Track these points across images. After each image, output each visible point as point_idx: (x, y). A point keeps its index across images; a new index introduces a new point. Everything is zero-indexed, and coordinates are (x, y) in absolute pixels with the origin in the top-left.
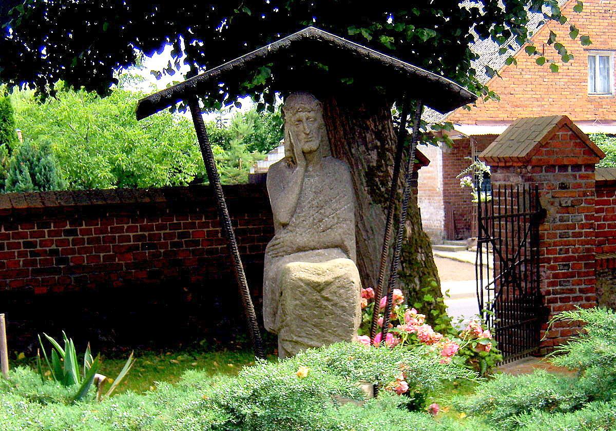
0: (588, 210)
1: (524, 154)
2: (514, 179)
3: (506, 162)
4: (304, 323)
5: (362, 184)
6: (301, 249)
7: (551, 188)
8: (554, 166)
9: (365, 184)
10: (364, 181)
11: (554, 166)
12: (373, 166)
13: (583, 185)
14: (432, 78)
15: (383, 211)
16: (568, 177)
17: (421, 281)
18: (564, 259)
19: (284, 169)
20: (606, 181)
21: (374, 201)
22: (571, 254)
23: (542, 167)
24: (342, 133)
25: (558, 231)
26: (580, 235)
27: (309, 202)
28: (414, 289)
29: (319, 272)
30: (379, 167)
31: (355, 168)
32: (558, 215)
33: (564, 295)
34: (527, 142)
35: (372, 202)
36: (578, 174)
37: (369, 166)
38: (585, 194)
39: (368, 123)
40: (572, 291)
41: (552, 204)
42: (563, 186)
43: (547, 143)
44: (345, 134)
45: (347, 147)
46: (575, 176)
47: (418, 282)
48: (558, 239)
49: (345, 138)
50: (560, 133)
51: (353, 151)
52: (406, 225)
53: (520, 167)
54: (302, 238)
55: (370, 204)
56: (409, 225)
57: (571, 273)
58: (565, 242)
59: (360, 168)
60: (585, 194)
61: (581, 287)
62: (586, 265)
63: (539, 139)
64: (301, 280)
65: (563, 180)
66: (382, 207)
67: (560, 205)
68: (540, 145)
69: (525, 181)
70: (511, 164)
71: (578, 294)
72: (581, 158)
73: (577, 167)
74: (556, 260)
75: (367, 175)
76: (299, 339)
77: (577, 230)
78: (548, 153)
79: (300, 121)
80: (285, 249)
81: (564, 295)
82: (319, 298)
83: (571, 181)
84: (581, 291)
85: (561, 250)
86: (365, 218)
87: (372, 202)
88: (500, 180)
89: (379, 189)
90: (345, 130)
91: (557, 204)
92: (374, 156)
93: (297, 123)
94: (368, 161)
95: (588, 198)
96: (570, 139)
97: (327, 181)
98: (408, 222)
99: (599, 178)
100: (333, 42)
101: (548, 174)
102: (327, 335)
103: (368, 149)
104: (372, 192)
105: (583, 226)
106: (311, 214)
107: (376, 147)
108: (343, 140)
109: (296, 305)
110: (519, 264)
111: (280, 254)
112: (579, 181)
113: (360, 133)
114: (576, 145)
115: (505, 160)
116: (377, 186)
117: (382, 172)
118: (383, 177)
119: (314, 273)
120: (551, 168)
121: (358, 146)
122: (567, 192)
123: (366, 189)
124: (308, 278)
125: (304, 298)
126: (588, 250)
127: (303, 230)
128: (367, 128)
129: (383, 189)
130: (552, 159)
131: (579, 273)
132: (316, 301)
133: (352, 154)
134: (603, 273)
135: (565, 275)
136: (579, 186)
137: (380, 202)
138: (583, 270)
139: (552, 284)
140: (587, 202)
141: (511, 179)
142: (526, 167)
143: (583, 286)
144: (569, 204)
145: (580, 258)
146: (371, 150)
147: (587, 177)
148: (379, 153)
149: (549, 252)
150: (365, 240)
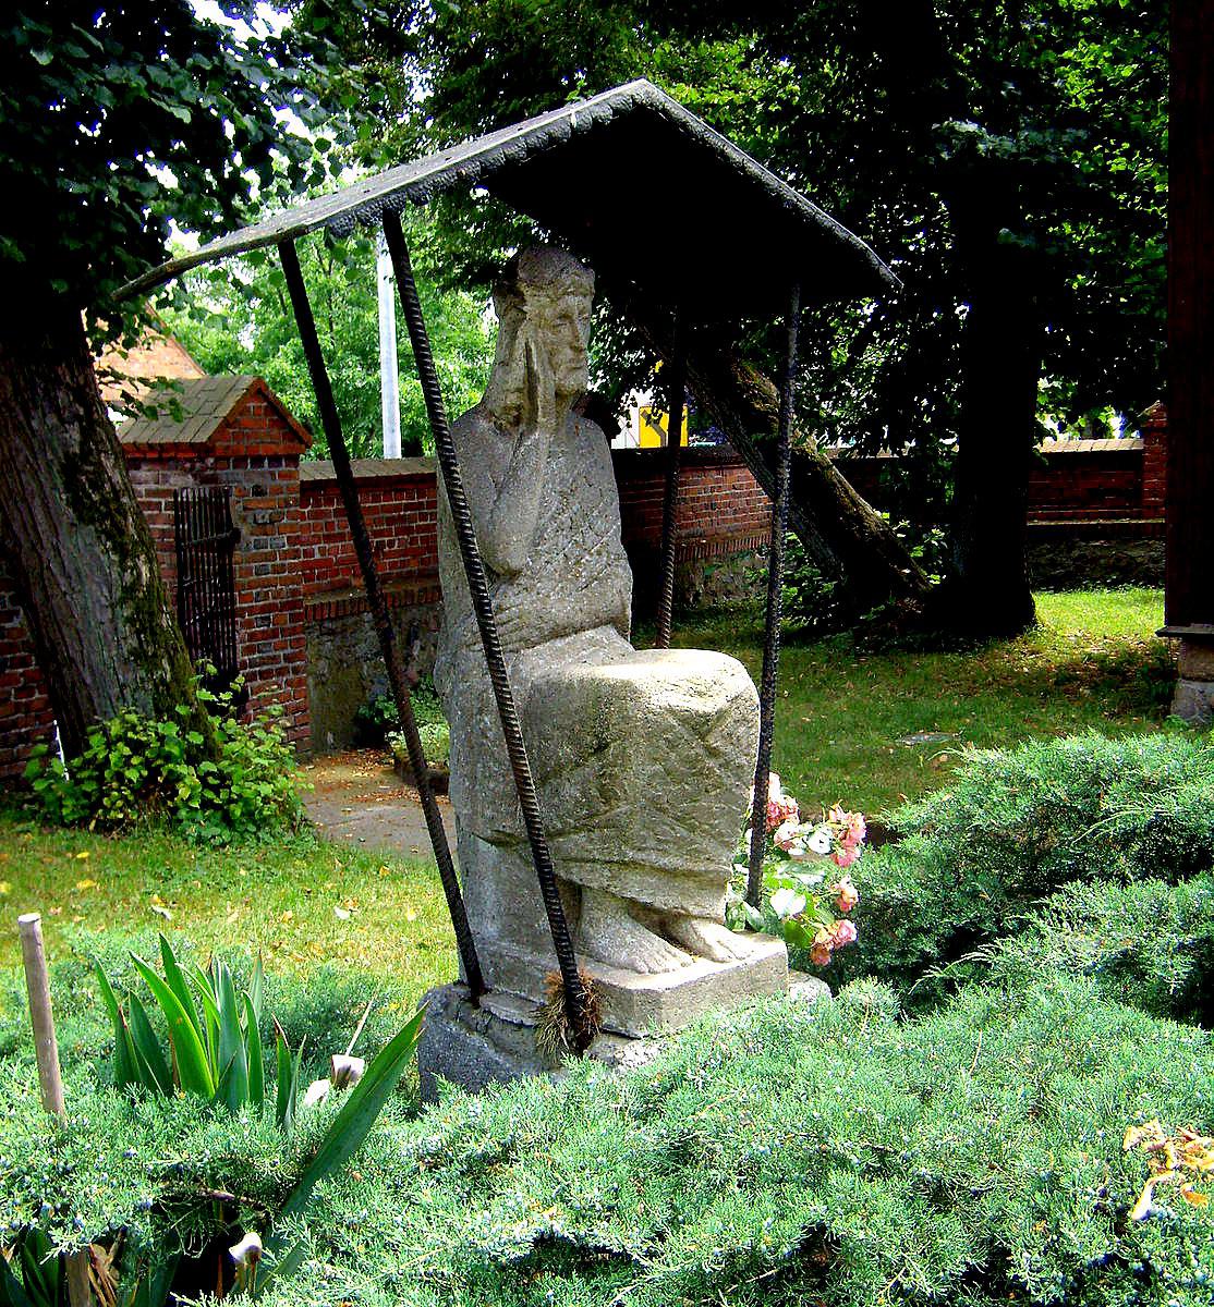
0: (292, 528)
1: (203, 438)
2: (179, 481)
3: (160, 453)
4: (659, 816)
5: (55, 487)
6: (559, 632)
7: (243, 493)
8: (244, 459)
9: (61, 487)
10: (59, 481)
11: (244, 459)
12: (75, 454)
13: (284, 490)
14: (840, 234)
15: (99, 538)
16: (262, 476)
17: (172, 664)
18: (263, 609)
19: (491, 437)
20: (401, 476)
21: (81, 519)
22: (271, 601)
23: (228, 460)
24: (10, 388)
25: (253, 565)
26: (282, 568)
27: (553, 518)
28: (163, 680)
29: (700, 688)
30: (86, 454)
31: (39, 456)
32: (253, 538)
33: (265, 668)
34: (201, 420)
35: (76, 522)
36: (276, 470)
37: (66, 454)
38: (287, 505)
39: (60, 372)
40: (275, 659)
41: (244, 519)
42: (258, 491)
43: (236, 421)
44: (17, 391)
45: (21, 418)
46: (272, 474)
47: (168, 667)
48: (255, 577)
49: (16, 400)
50: (252, 405)
51: (34, 424)
52: (140, 563)
53: (190, 460)
54: (561, 608)
55: (73, 525)
56: (145, 563)
57: (273, 630)
58: (264, 580)
59: (50, 456)
60: (287, 505)
61: (286, 652)
62: (294, 618)
63: (224, 412)
64: (671, 711)
65: (258, 480)
66: (96, 530)
67: (255, 521)
68: (227, 423)
69: (202, 483)
70: (172, 454)
71: (283, 664)
72: (282, 445)
73: (275, 460)
74: (251, 610)
75: (64, 470)
76: (640, 856)
77: (278, 561)
78: (236, 437)
79: (565, 316)
80: (524, 633)
81: (265, 668)
82: (701, 751)
83: (268, 483)
84: (288, 658)
85: (258, 594)
86: (63, 552)
87: (76, 522)
88: (146, 482)
89: (89, 497)
90: (15, 385)
91: (250, 520)
92: (74, 434)
93: (558, 322)
94: (65, 445)
95: (292, 509)
96: (266, 414)
97: (582, 466)
98: (143, 557)
99: (305, 478)
100: (684, 125)
101: (237, 471)
102: (699, 839)
103: (62, 421)
104: (75, 503)
105: (285, 555)
106: (560, 547)
107: (77, 417)
108: (13, 404)
109: (654, 775)
110: (194, 624)
111: (510, 647)
112: (279, 482)
113: (46, 390)
114: (273, 424)
115: (163, 447)
116: (84, 490)
117: (91, 464)
118: (94, 473)
119: (692, 692)
120: (240, 462)
121: (44, 415)
122: (263, 501)
123: (64, 497)
124: (686, 706)
125: (673, 755)
126: (294, 593)
127: (550, 585)
128: (58, 382)
129: (95, 497)
130: (243, 447)
131: (283, 630)
132: (693, 762)
133: (31, 428)
134: (308, 628)
135: (265, 635)
136: (278, 491)
137: (92, 521)
138: (288, 625)
139: (249, 650)
140: (291, 516)
141: (172, 480)
142: (202, 460)
143: (289, 651)
144: (267, 519)
145: (285, 606)
146: (69, 423)
147: (289, 476)
148: (83, 431)
149: (243, 599)
150: (65, 593)
